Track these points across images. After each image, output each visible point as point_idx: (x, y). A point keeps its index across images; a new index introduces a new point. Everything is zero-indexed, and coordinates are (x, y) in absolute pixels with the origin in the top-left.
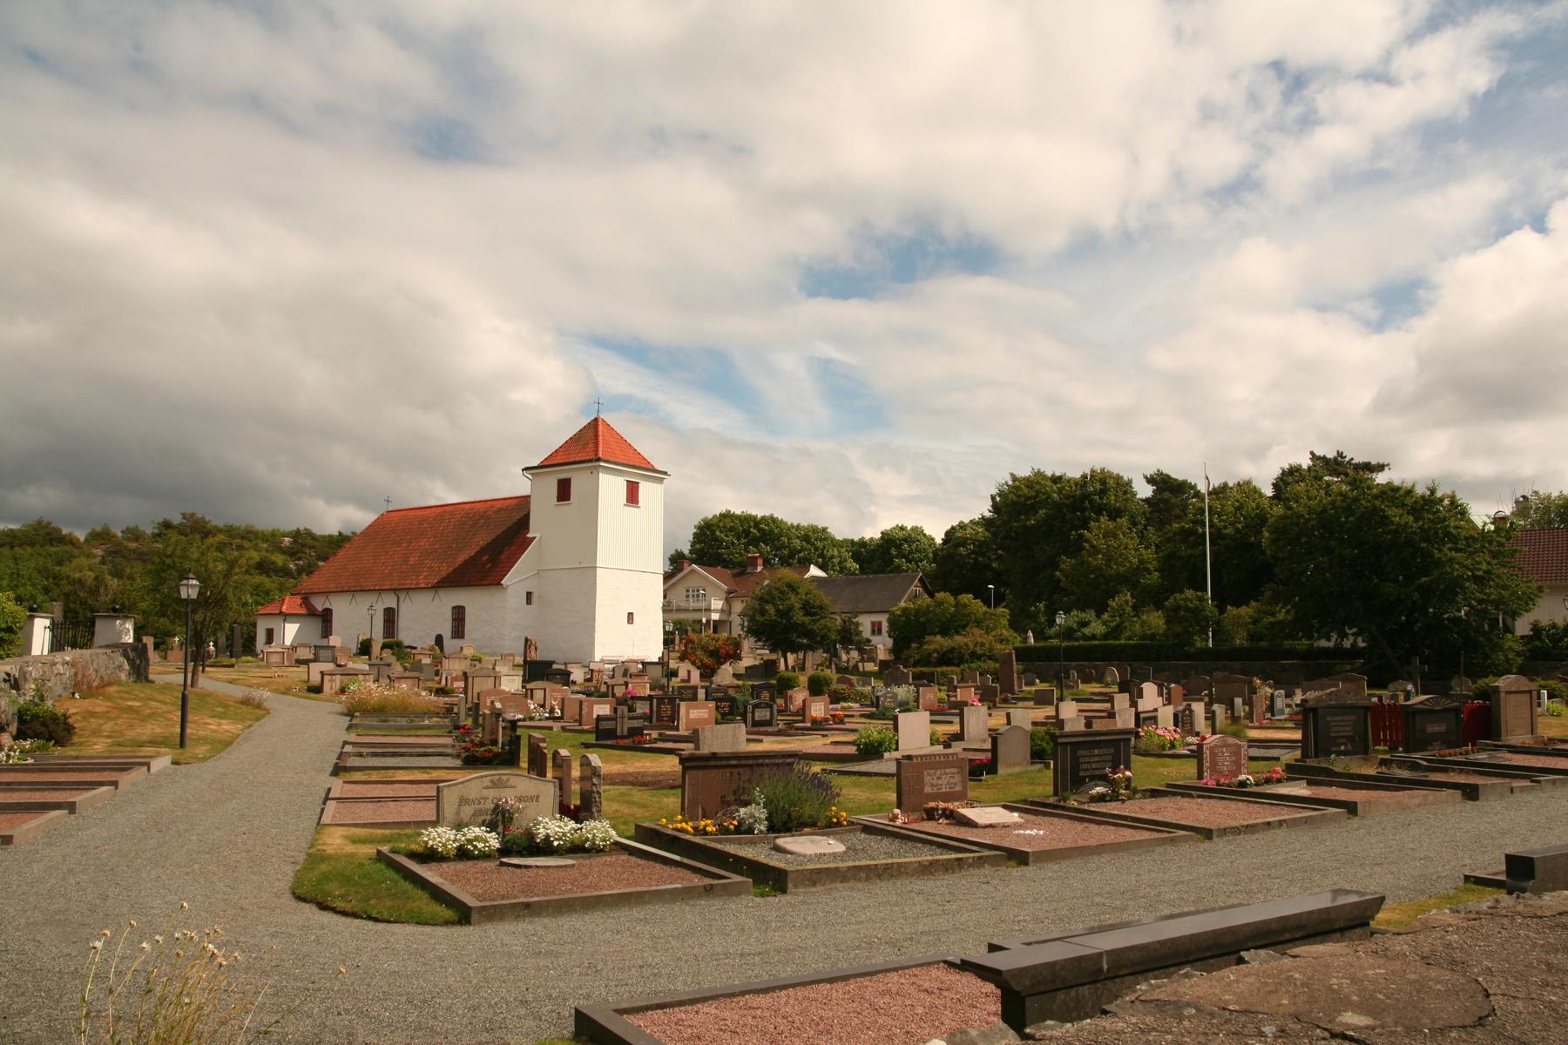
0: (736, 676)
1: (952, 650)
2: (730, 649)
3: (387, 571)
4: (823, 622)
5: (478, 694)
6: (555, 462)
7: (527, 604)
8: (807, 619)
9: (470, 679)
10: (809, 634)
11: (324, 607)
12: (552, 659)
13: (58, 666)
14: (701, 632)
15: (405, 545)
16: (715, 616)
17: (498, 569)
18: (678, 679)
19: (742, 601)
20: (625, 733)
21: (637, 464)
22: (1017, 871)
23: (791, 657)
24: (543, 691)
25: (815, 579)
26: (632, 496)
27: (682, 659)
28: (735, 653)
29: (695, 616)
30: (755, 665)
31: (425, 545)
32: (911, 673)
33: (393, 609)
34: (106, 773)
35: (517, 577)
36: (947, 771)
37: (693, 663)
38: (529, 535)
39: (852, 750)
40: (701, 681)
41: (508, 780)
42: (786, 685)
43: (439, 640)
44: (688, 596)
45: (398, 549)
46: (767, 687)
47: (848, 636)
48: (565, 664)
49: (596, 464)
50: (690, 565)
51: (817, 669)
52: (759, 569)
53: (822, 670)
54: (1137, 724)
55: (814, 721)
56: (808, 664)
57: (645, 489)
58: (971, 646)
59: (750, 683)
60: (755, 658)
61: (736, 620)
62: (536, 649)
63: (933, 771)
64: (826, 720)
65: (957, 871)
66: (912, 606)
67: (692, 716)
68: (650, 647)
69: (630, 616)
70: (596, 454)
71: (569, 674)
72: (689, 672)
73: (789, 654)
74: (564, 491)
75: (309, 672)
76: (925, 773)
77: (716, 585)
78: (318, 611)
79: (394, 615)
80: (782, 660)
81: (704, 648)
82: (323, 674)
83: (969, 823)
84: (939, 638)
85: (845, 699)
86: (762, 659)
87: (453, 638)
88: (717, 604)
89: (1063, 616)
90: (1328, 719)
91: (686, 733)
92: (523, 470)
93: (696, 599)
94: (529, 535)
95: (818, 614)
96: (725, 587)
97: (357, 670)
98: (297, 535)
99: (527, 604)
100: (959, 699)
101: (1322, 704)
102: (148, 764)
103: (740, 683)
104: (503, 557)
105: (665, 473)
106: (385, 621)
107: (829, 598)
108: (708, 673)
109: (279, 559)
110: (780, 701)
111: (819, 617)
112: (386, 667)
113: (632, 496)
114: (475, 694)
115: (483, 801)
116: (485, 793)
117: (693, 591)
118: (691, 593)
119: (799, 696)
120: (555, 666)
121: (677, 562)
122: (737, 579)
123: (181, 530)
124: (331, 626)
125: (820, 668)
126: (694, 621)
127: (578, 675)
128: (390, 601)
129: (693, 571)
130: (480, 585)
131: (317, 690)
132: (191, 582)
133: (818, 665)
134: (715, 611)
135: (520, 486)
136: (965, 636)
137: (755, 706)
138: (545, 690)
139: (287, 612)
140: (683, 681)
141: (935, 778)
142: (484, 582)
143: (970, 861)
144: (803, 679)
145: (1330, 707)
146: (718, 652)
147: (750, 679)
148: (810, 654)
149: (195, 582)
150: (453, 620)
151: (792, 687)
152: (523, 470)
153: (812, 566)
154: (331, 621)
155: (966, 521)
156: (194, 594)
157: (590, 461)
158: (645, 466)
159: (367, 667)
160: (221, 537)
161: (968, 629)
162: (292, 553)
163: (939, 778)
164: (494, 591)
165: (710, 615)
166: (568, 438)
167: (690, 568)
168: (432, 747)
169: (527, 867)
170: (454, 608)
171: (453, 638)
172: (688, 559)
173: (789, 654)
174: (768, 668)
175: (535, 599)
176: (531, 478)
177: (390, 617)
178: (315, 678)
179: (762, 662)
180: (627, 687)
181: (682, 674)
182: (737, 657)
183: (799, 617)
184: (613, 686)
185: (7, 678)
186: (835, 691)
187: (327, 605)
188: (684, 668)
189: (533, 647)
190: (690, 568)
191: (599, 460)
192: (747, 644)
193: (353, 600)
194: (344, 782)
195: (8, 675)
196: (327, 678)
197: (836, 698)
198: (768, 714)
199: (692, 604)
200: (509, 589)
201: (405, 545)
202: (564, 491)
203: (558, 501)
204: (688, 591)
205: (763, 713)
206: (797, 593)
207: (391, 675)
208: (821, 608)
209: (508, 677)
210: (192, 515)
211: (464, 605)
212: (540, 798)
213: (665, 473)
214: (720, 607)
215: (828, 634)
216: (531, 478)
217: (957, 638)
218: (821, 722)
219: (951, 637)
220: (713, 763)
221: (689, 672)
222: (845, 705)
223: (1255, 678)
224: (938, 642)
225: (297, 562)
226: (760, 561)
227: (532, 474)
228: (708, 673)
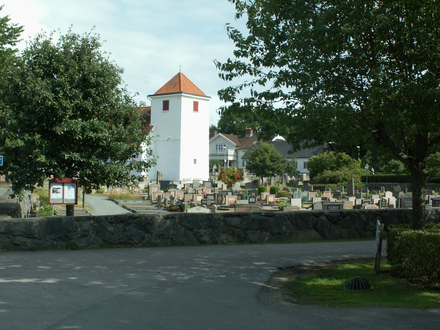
0: (241, 187)
1: (334, 177)
2: (238, 175)
4: (278, 164)
8: (271, 164)
10: (273, 170)
14: (224, 166)
16: (231, 158)
18: (217, 188)
19: (243, 151)
20: (210, 205)
21: (198, 94)
23: (265, 179)
26: (196, 107)
27: (219, 180)
28: (241, 177)
29: (221, 158)
30: (249, 183)
32: (312, 187)
37: (223, 181)
39: (278, 209)
40: (227, 189)
42: (261, 191)
43: (241, 89)
44: (217, 148)
46: (254, 191)
47: (291, 171)
49: (180, 94)
50: (218, 133)
51: (276, 184)
52: (251, 135)
53: (278, 185)
54: (362, 203)
55: (270, 203)
56: (272, 182)
57: (202, 104)
58: (343, 175)
59: (248, 190)
60: (249, 179)
61: (240, 161)
64: (274, 202)
65: (90, 40)
66: (318, 157)
67: (230, 200)
69: (195, 160)
70: (180, 89)
72: (222, 185)
73: (264, 178)
74: (166, 106)
77: (230, 143)
80: (261, 180)
81: (228, 175)
84: (329, 171)
85: (283, 196)
86: (252, 179)
88: (231, 152)
90: (405, 201)
91: (228, 205)
92: (147, 96)
93: (221, 150)
95: (276, 161)
100: (324, 197)
101: (403, 197)
103: (244, 190)
105: (210, 97)
107: (281, 154)
108: (230, 185)
110: (259, 197)
111: (276, 162)
113: (196, 107)
117: (220, 146)
118: (218, 147)
119: (264, 195)
121: (212, 130)
122: (240, 139)
125: (277, 184)
126: (220, 161)
129: (219, 136)
133: (277, 182)
136: (340, 171)
137: (250, 197)
138: (175, 192)
140: (219, 189)
144: (268, 188)
145: (405, 198)
146: (234, 177)
147: (248, 188)
148: (273, 178)
151: (263, 191)
152: (147, 96)
157: (178, 93)
158: (200, 94)
161: (343, 168)
165: (228, 158)
167: (218, 135)
172: (216, 130)
173: (264, 178)
174: (255, 182)
179: (252, 181)
180: (203, 191)
181: (219, 186)
182: (242, 179)
183: (269, 163)
186: (280, 193)
188: (220, 184)
189: (160, 175)
190: (218, 135)
191: (181, 92)
192: (245, 174)
197: (279, 195)
198: (254, 200)
199: (219, 152)
202: (166, 106)
204: (217, 146)
205: (252, 200)
206: (268, 153)
208: (277, 158)
213: (210, 97)
214: (233, 154)
215: (281, 170)
216: (151, 99)
217: (338, 172)
218: (272, 203)
219: (335, 171)
220: (241, 206)
221: (222, 185)
222: (282, 198)
223: (433, 191)
224: (328, 173)
226: (252, 131)
227: (151, 98)
228: (230, 185)
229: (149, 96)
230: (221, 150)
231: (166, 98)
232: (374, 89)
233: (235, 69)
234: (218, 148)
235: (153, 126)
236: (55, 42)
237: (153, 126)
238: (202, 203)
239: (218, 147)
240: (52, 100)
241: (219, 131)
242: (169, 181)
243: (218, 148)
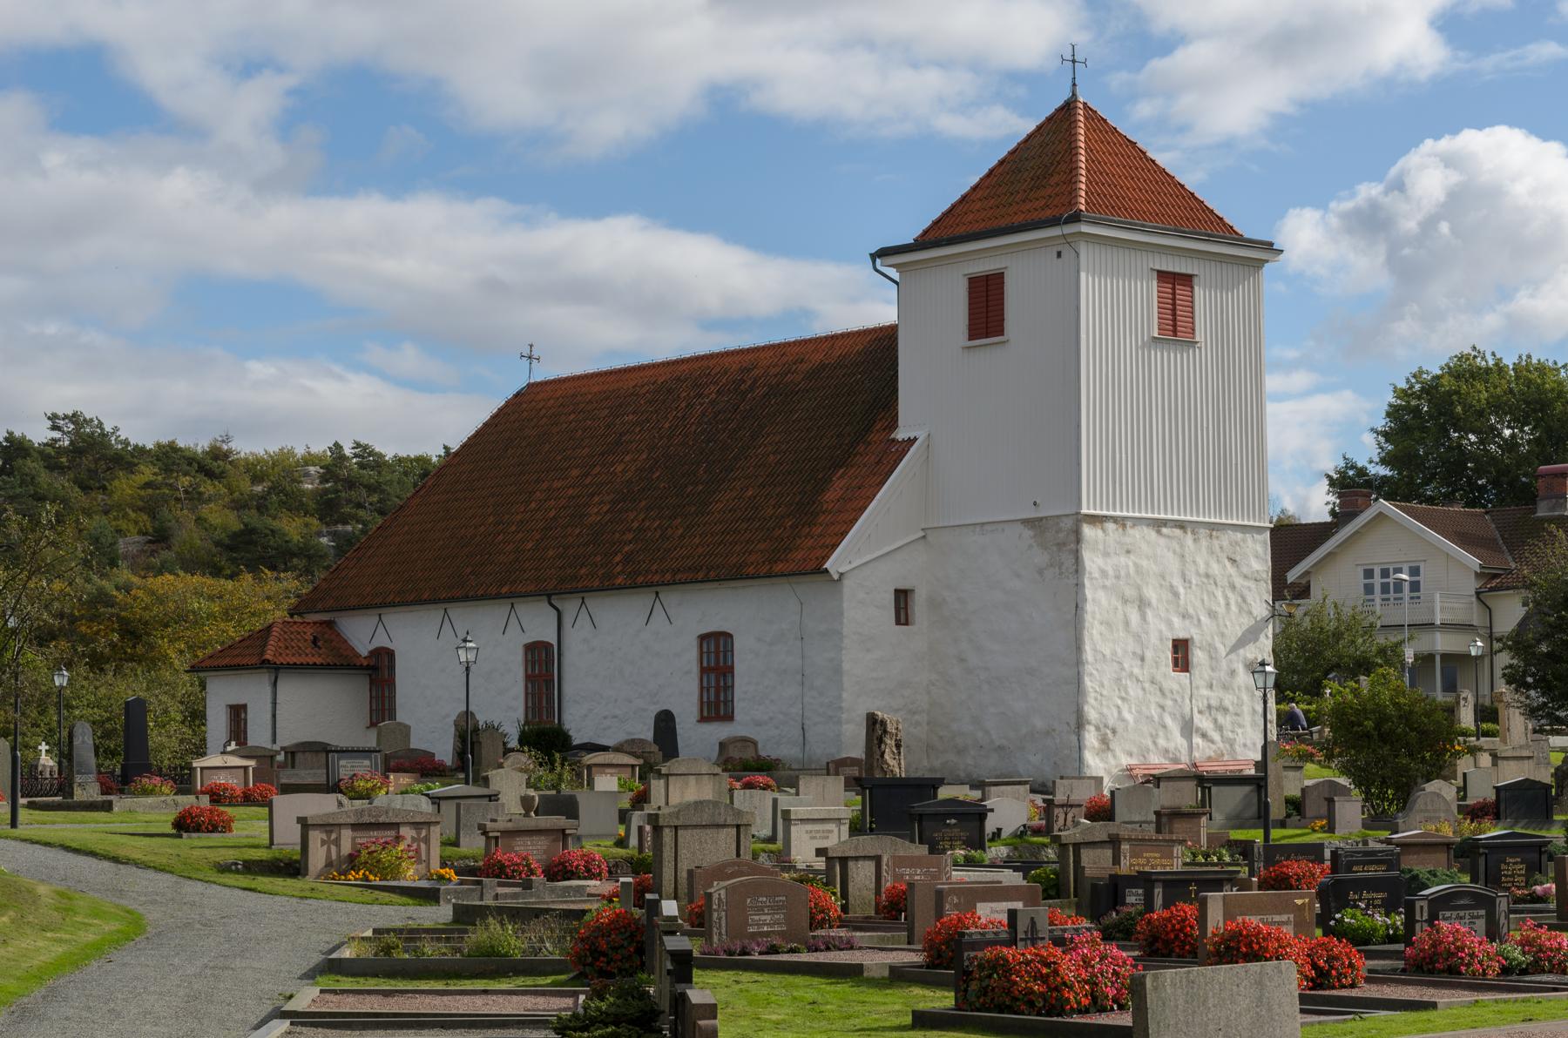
6: (961, 230)
7: (898, 622)
9: (668, 835)
11: (376, 644)
12: (938, 776)
15: (575, 472)
31: (624, 471)
33: (547, 646)
38: (901, 434)
43: (665, 724)
44: (1369, 589)
45: (557, 484)
48: (979, 785)
49: (1069, 229)
62: (898, 746)
71: (981, 815)
78: (358, 656)
79: (550, 662)
82: (305, 824)
87: (703, 719)
89: (65, 673)
92: (874, 257)
93: (1392, 595)
94: (901, 434)
96: (1474, 562)
97: (397, 812)
99: (898, 622)
106: (529, 678)
109: (292, 528)
112: (485, 802)
114: (683, 875)
117: (1385, 573)
118: (1377, 580)
120: (944, 793)
124: (392, 698)
128: (537, 622)
129: (1381, 516)
130: (769, 576)
131: (292, 868)
138: (877, 860)
142: (779, 567)
150: (704, 671)
152: (874, 257)
154: (390, 682)
155: (139, 432)
159: (425, 805)
162: (327, 508)
166: (994, 162)
170: (703, 638)
171: (703, 719)
175: (919, 607)
178: (288, 836)
184: (1077, 847)
187: (381, 641)
189: (890, 742)
191: (1076, 218)
193: (513, 619)
196: (316, 837)
200: (846, 582)
201: (575, 472)
203: (971, 337)
204: (1369, 574)
207: (489, 825)
209: (809, 827)
210: (74, 418)
211: (725, 628)
229: (883, 253)
230: (1392, 595)
231: (981, 257)
232: (1045, 845)
234: (1377, 589)
235: (915, 439)
237: (915, 439)
239: (1377, 580)
242: (934, 784)
243: (1377, 589)
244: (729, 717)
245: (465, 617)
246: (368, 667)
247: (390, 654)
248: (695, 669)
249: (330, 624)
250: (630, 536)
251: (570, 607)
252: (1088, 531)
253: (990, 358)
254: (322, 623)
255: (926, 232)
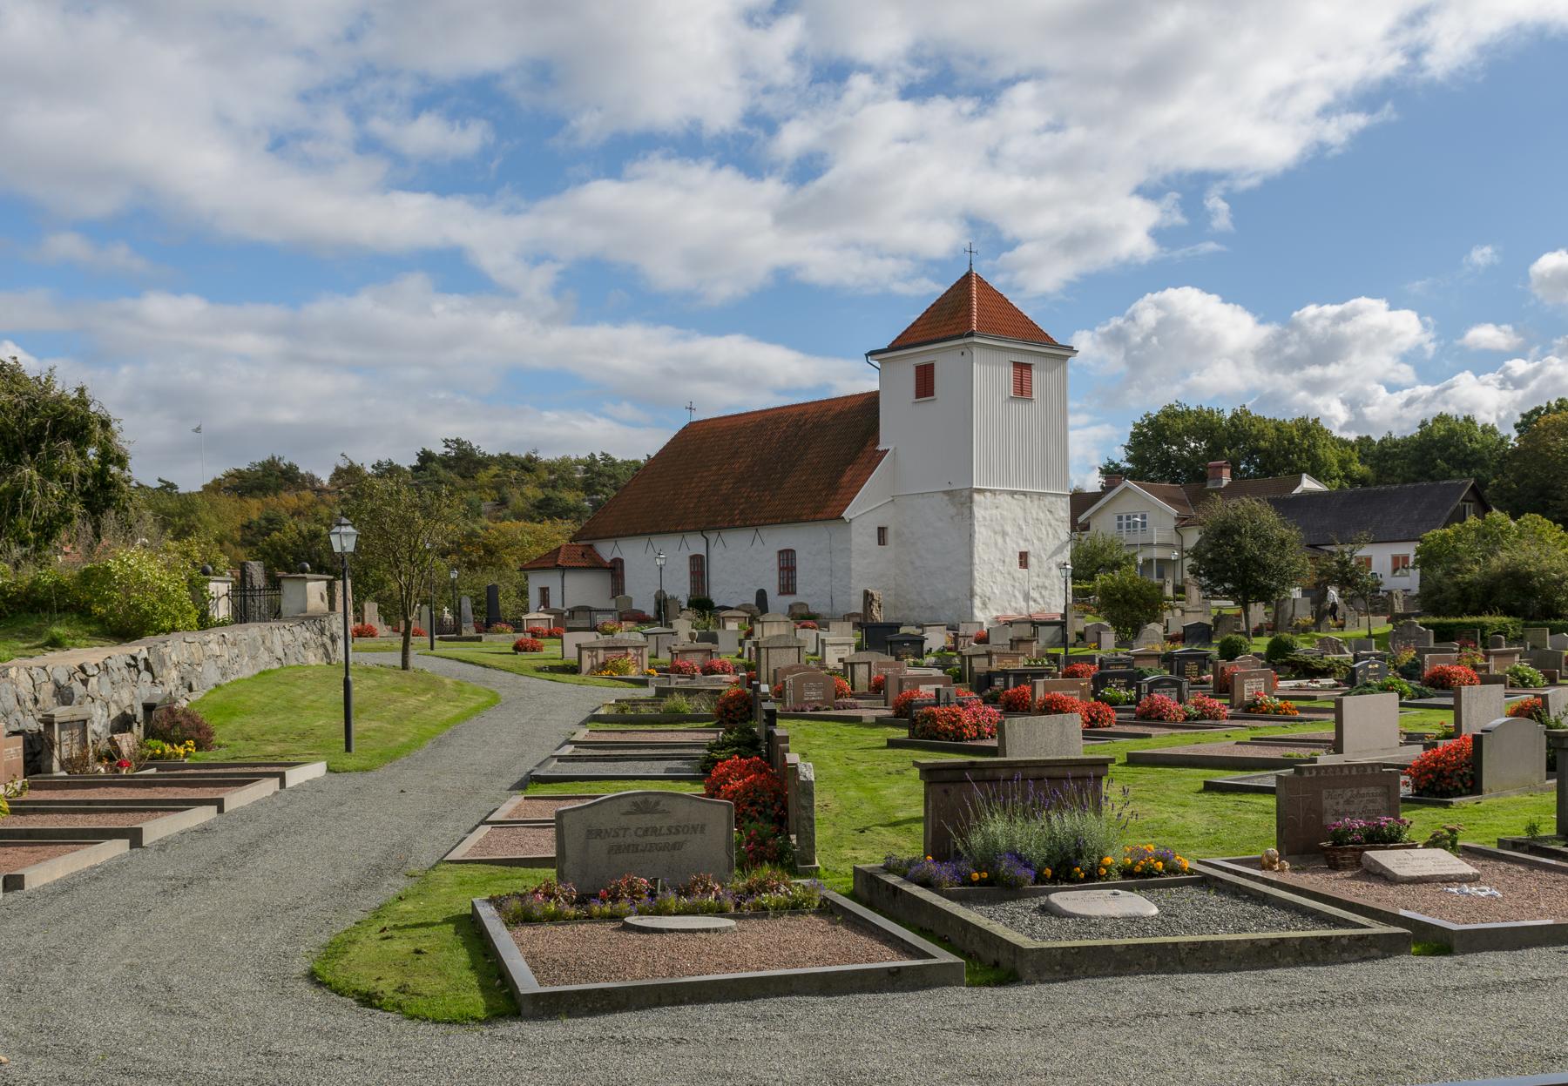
3: (692, 505)
5: (775, 671)
6: (912, 341)
9: (763, 652)
11: (614, 556)
13: (211, 645)
15: (714, 468)
17: (839, 497)
22: (1403, 971)
24: (867, 666)
25: (1310, 496)
26: (1022, 389)
33: (702, 557)
34: (112, 789)
35: (864, 508)
36: (1363, 791)
38: (881, 448)
41: (657, 803)
43: (761, 596)
44: (1120, 526)
63: (1339, 791)
68: (1052, 598)
74: (925, 383)
75: (562, 645)
76: (1325, 793)
83: (1386, 878)
87: (781, 594)
92: (867, 355)
94: (881, 448)
98: (590, 465)
99: (880, 544)
102: (282, 777)
104: (845, 479)
106: (692, 573)
114: (771, 672)
115: (621, 833)
116: (624, 821)
117: (1128, 518)
118: (1124, 521)
120: (903, 630)
123: (445, 462)
124: (623, 584)
127: (936, 639)
128: (696, 545)
132: (344, 529)
134: (1207, 552)
135: (866, 380)
138: (869, 663)
139: (565, 565)
141: (1341, 801)
142: (819, 516)
143: (1345, 942)
149: (350, 529)
150: (781, 569)
152: (867, 355)
153: (1305, 475)
156: (350, 545)
157: (960, 336)
160: (495, 470)
163: (1348, 802)
164: (833, 526)
168: (645, 747)
169: (660, 931)
170: (780, 552)
171: (781, 594)
175: (890, 536)
176: (878, 365)
177: (699, 567)
178: (571, 655)
185: (133, 663)
187: (617, 555)
191: (971, 334)
193: (650, 546)
194: (525, 798)
195: (134, 658)
196: (585, 654)
200: (853, 524)
201: (714, 468)
202: (925, 383)
203: (917, 397)
204: (1120, 518)
207: (673, 647)
210: (457, 441)
212: (706, 828)
216: (878, 365)
225: (595, 497)
229: (872, 353)
231: (922, 355)
233: (1266, 331)
236: (1376, 438)
238: (986, 660)
239: (1124, 521)
240: (491, 524)
241: (1132, 474)
244: (794, 593)
245: (659, 542)
246: (610, 568)
247: (621, 561)
248: (777, 568)
249: (590, 546)
250: (743, 500)
251: (713, 536)
252: (976, 497)
253: (927, 408)
254: (586, 545)
255: (894, 342)
